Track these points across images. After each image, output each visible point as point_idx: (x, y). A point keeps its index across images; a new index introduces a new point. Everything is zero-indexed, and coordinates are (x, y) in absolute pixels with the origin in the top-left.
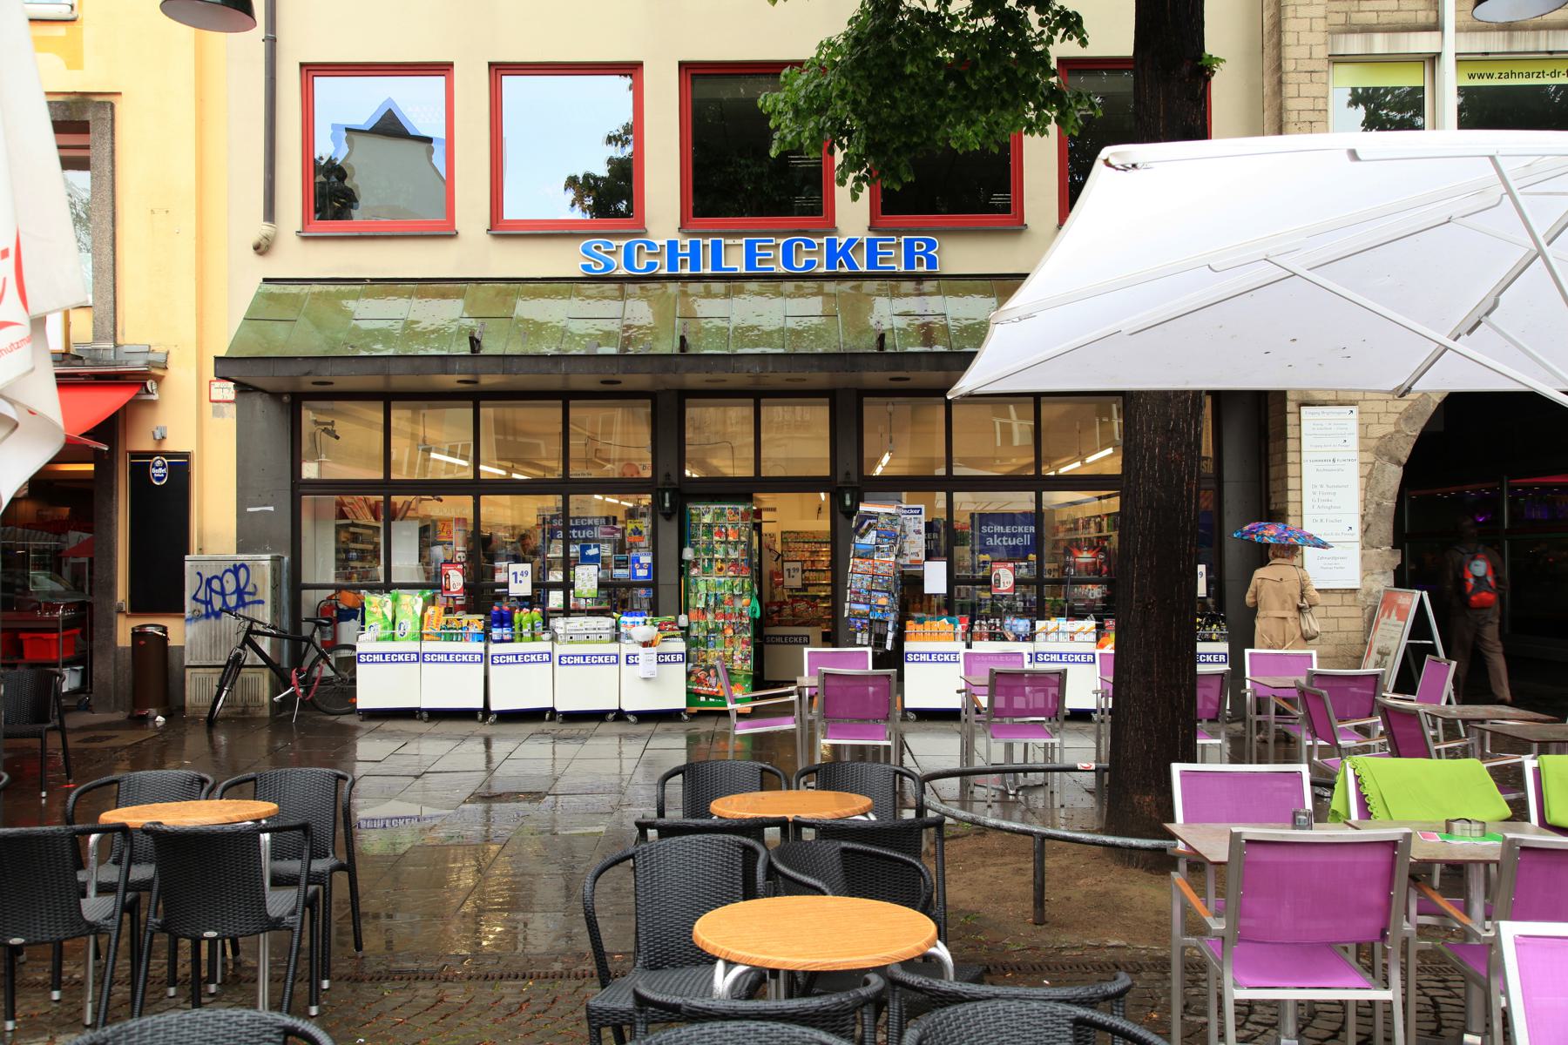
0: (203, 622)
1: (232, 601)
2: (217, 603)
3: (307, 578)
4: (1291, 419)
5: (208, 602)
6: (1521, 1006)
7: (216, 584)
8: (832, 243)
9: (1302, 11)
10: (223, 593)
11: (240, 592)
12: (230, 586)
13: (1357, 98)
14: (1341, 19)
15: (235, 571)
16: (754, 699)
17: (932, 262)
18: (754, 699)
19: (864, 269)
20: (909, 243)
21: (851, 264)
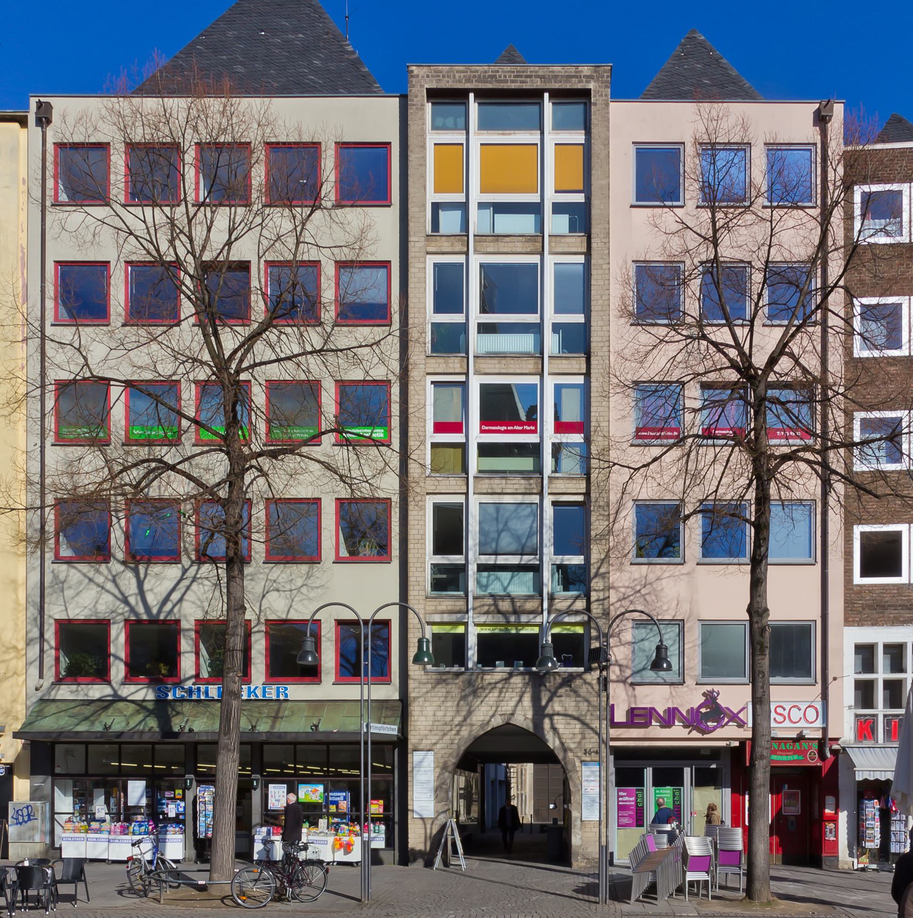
0: (15, 826)
1: (26, 818)
2: (21, 819)
3: (56, 810)
4: (410, 756)
5: (17, 819)
6: (398, 302)
7: (20, 813)
8: (249, 688)
9: (416, 588)
10: (22, 816)
11: (29, 815)
12: (25, 813)
13: (432, 383)
14: (433, 608)
15: (27, 807)
16: (366, 743)
17: (286, 695)
18: (366, 743)
19: (261, 698)
20: (278, 688)
21: (257, 696)
